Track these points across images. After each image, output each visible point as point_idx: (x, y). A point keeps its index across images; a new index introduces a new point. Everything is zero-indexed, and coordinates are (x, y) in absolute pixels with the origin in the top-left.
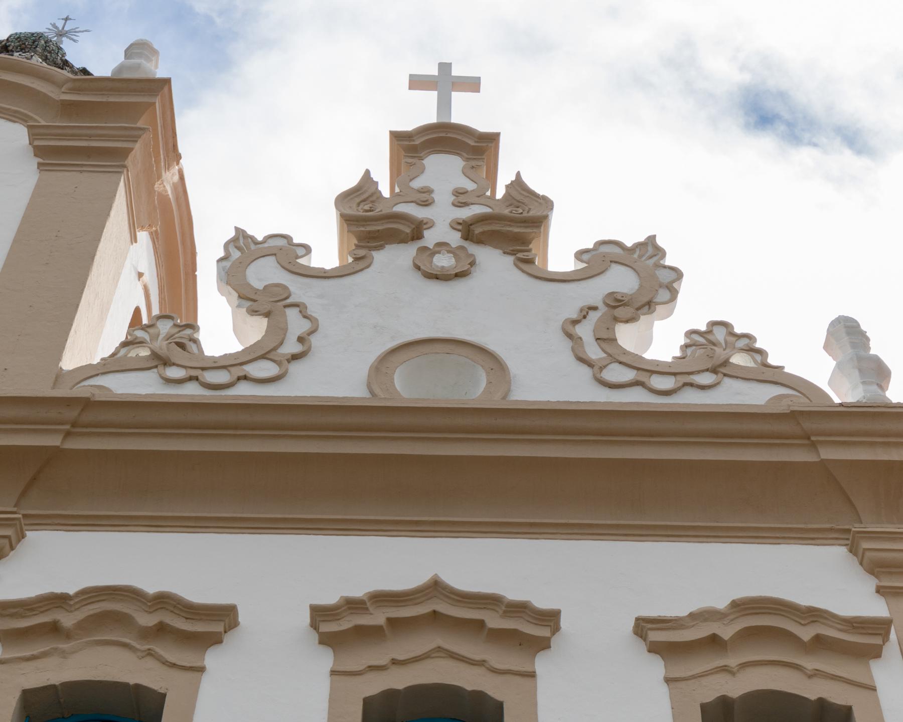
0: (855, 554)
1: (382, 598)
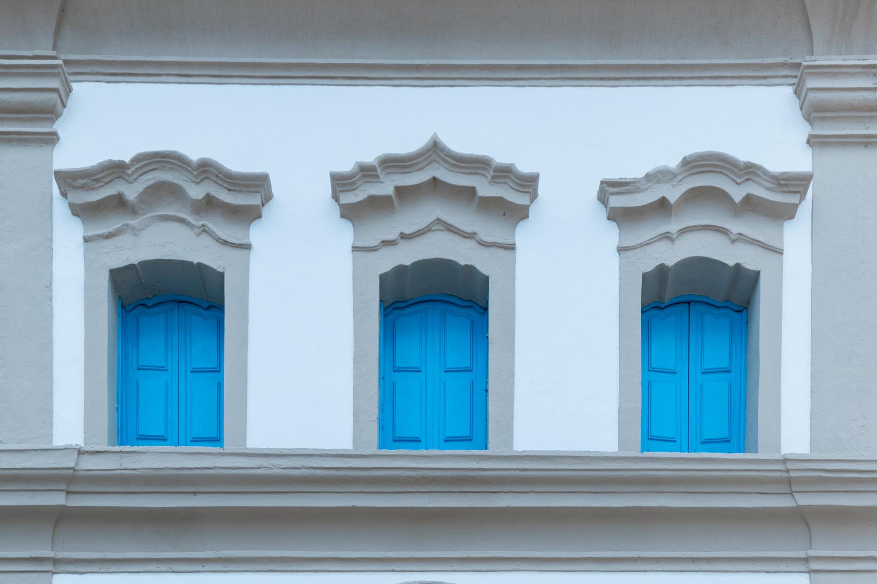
0: (799, 97)
1: (393, 164)
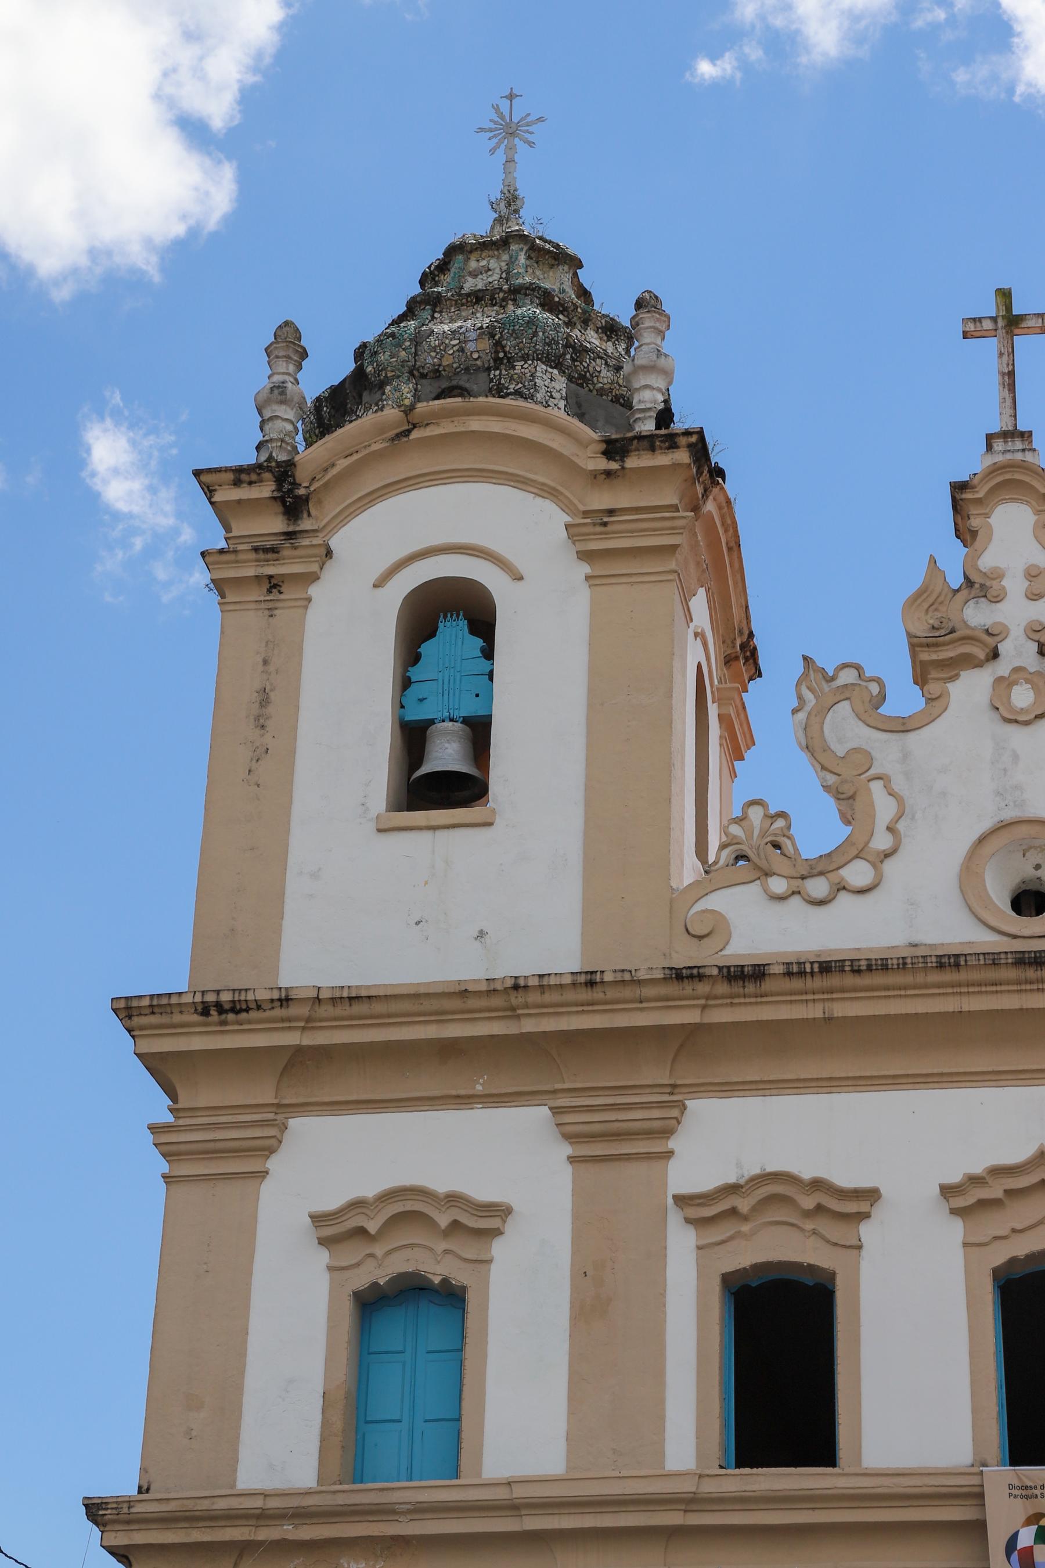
1: (998, 1171)
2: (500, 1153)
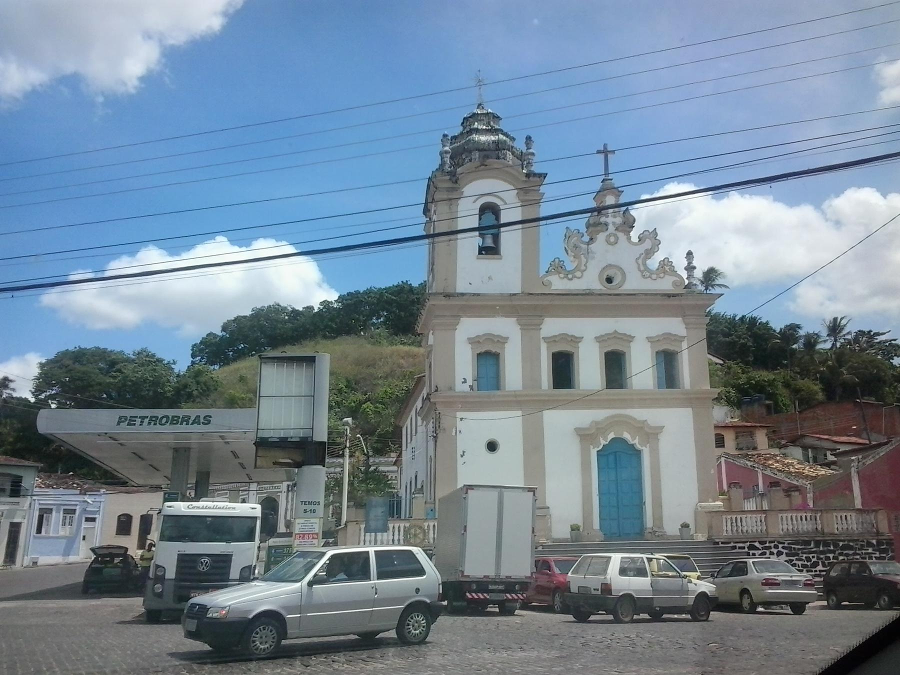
2: (506, 327)
